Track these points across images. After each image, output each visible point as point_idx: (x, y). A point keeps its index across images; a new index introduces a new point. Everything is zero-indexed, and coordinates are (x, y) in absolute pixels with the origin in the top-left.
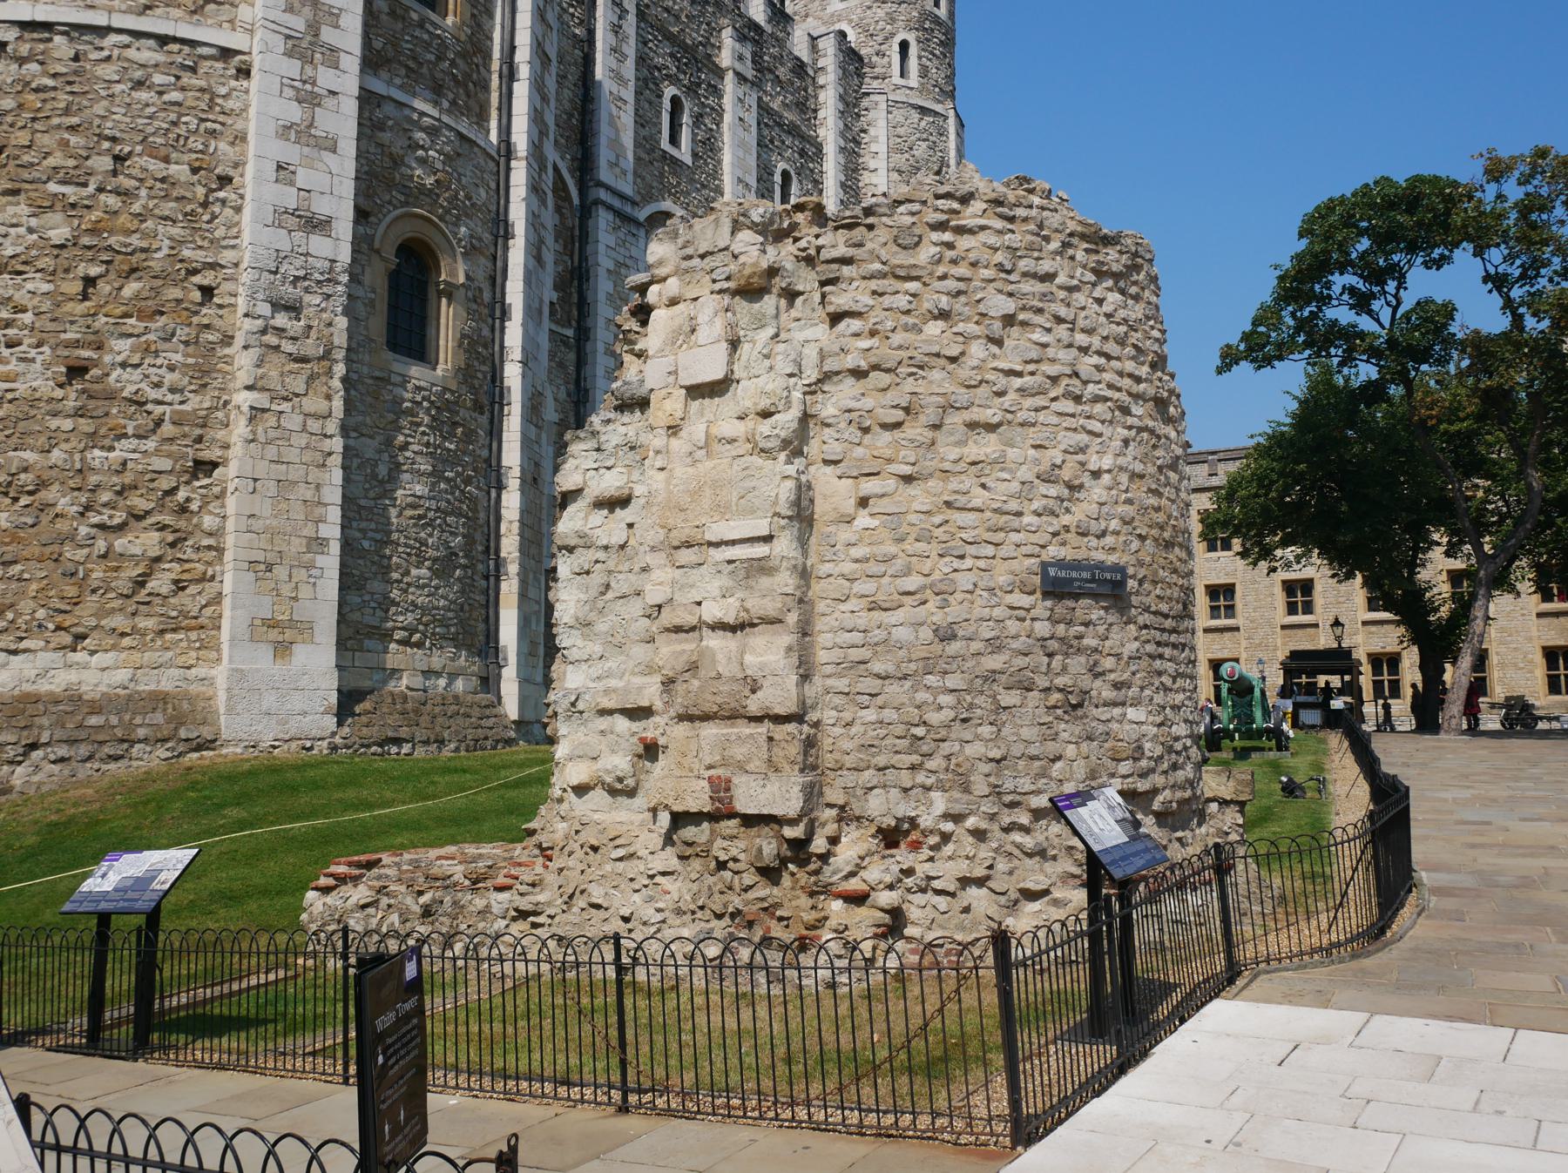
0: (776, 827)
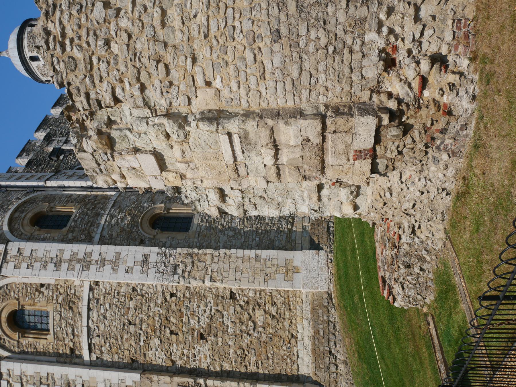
0: (382, 128)
